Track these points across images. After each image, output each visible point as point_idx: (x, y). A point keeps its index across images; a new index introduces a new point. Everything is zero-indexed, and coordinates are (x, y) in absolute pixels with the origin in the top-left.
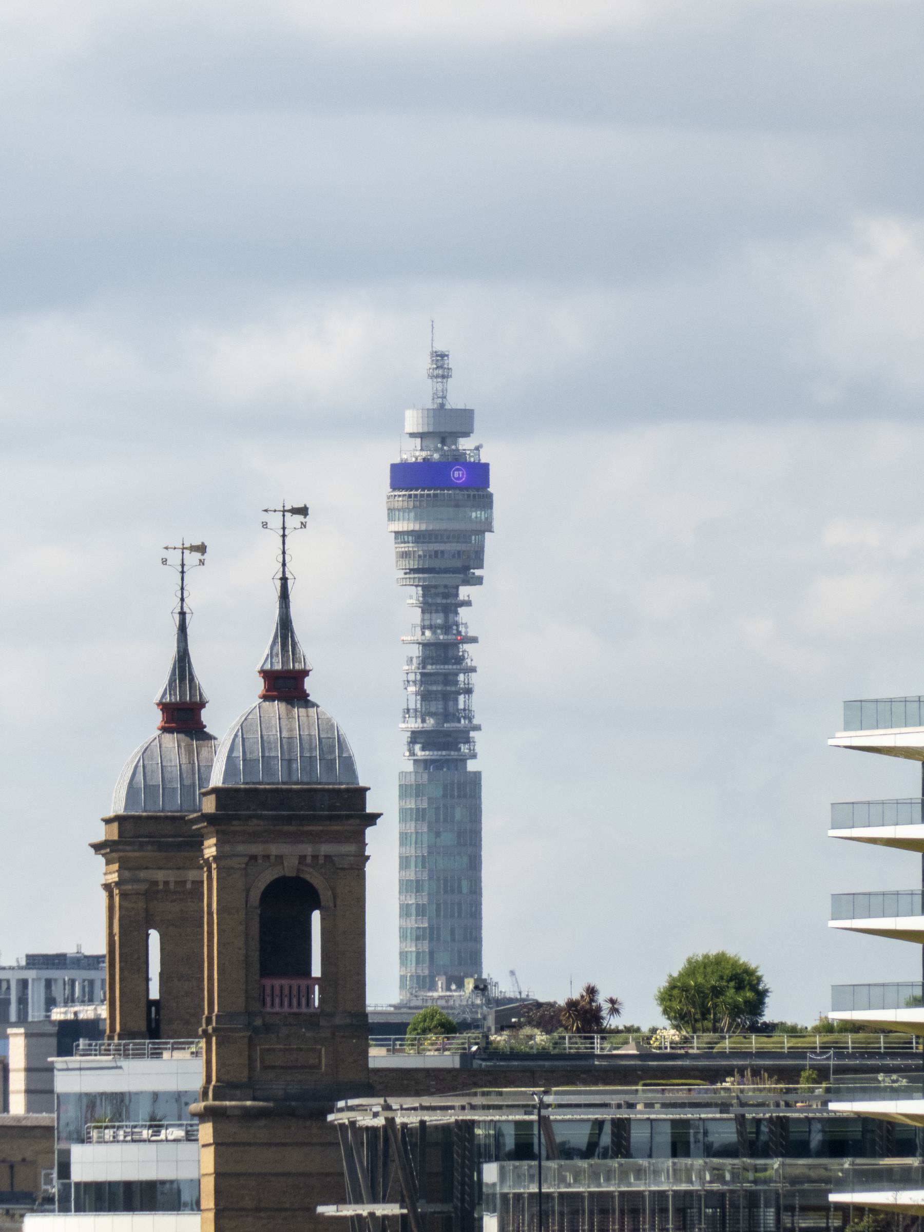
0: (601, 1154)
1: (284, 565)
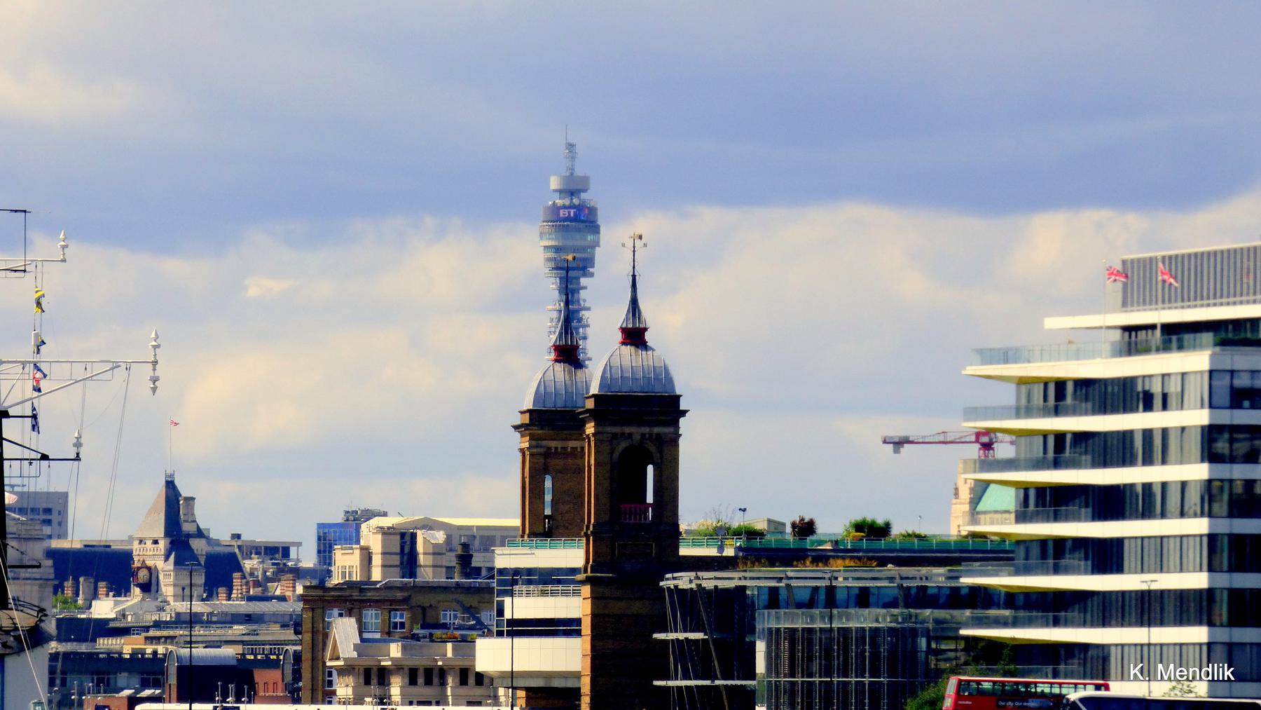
1: (634, 267)
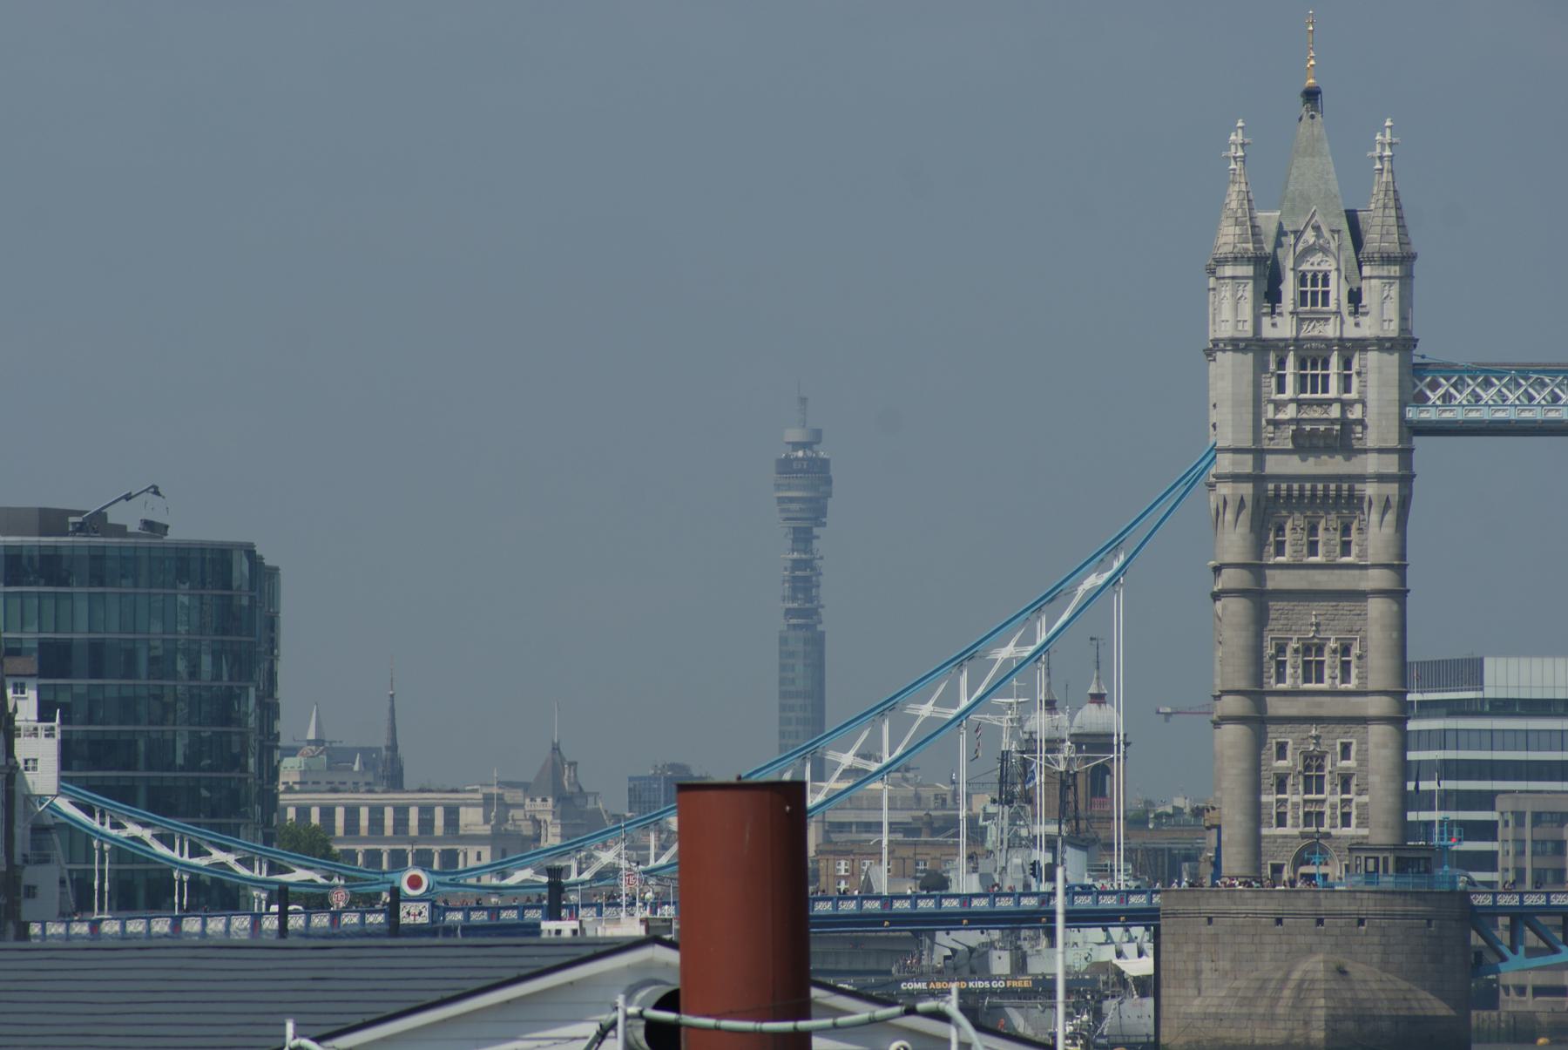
0: (1187, 852)
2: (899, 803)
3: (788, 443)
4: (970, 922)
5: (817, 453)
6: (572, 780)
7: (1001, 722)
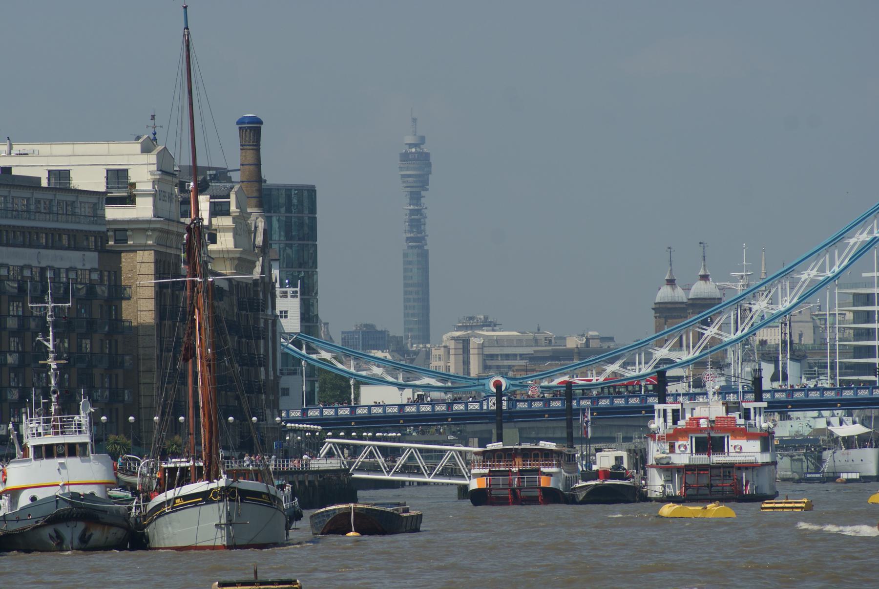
2: (525, 343)
3: (406, 144)
4: (842, 405)
5: (423, 149)
6: (326, 333)
7: (736, 286)
